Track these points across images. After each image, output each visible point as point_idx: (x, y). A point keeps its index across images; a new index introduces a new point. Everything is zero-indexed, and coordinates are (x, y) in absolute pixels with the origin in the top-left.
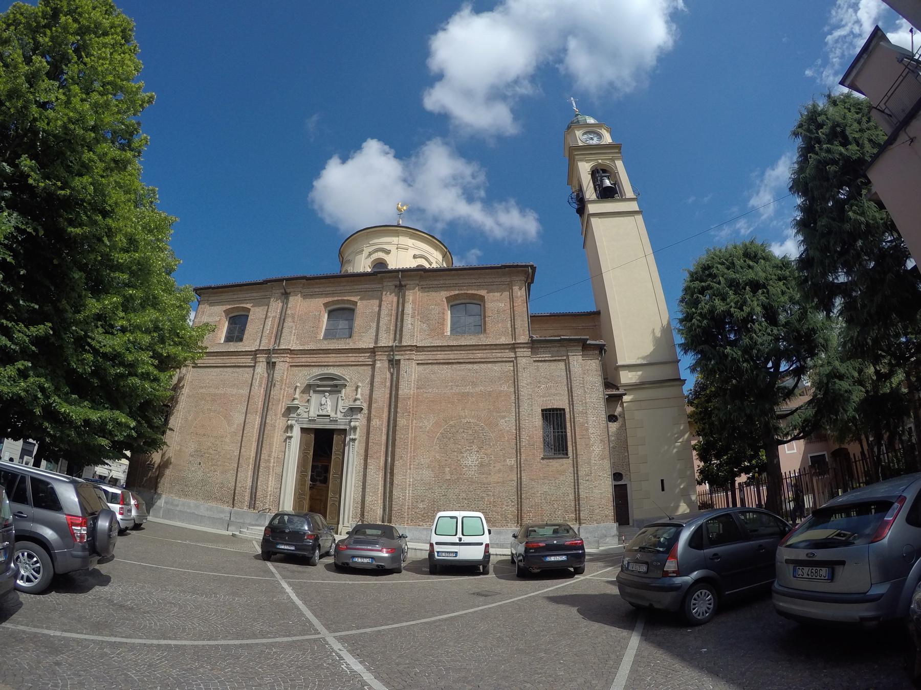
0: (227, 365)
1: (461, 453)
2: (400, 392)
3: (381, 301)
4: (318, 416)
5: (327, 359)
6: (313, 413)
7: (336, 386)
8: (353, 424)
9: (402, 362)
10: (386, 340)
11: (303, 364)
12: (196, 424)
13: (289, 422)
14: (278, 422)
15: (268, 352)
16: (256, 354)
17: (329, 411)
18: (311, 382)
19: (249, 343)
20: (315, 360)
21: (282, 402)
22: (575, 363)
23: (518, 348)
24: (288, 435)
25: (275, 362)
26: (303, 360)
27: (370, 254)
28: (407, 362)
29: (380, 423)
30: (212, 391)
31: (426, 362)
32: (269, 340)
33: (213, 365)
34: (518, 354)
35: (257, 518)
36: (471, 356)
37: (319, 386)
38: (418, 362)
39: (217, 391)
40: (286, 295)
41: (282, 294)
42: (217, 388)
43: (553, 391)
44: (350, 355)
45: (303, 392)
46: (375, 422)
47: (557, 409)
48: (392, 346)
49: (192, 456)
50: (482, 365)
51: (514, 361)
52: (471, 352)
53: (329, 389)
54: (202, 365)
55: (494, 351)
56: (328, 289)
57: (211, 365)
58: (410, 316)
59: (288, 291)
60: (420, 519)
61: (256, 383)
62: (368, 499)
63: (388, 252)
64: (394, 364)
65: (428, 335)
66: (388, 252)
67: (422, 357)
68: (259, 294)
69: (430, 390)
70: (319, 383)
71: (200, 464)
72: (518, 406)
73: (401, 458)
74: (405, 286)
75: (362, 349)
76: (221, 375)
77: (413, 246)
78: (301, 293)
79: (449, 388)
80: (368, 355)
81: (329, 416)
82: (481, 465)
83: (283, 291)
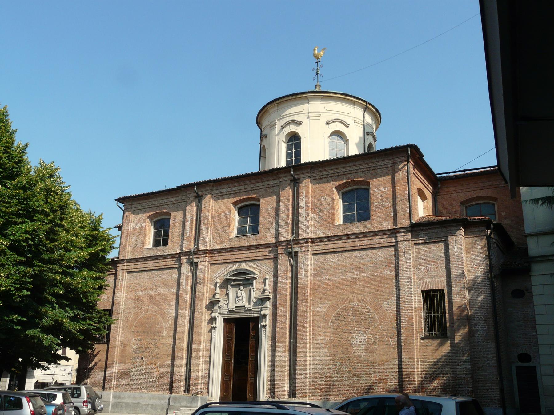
0: (157, 268)
1: (351, 333)
2: (299, 281)
3: (279, 197)
4: (236, 307)
5: (239, 256)
6: (232, 305)
7: (248, 279)
8: (263, 312)
9: (300, 254)
10: (286, 235)
11: (220, 261)
12: (137, 323)
13: (213, 315)
14: (203, 315)
15: (189, 253)
16: (181, 257)
17: (245, 302)
18: (228, 277)
19: (173, 248)
20: (230, 257)
21: (206, 297)
22: (454, 243)
23: (398, 232)
24: (212, 326)
25: (197, 262)
26: (220, 258)
27: (283, 128)
28: (304, 254)
29: (285, 310)
30: (148, 292)
31: (319, 252)
32: (190, 243)
33: (145, 269)
34: (399, 239)
35: (191, 400)
36: (358, 244)
37: (234, 281)
38: (313, 252)
39: (151, 292)
40: (199, 198)
41: (196, 197)
42: (151, 289)
43: (433, 273)
44: (258, 250)
45: (221, 287)
46: (280, 310)
47: (436, 290)
48: (290, 240)
49: (135, 352)
50: (370, 252)
51: (395, 246)
52: (357, 240)
53: (241, 282)
54: (135, 270)
55: (377, 237)
56: (234, 189)
57: (143, 269)
58: (304, 209)
59: (200, 193)
60: (319, 394)
61: (183, 282)
62: (277, 377)
63: (299, 123)
64: (294, 256)
65: (321, 226)
66: (299, 123)
67: (318, 247)
68: (176, 199)
69: (324, 277)
70: (234, 278)
71: (142, 358)
72: (398, 289)
73: (302, 339)
74: (299, 179)
75: (267, 244)
76: (153, 277)
77: (325, 111)
78: (211, 194)
79: (340, 275)
80: (270, 249)
81: (244, 306)
82: (368, 344)
83: (195, 194)
